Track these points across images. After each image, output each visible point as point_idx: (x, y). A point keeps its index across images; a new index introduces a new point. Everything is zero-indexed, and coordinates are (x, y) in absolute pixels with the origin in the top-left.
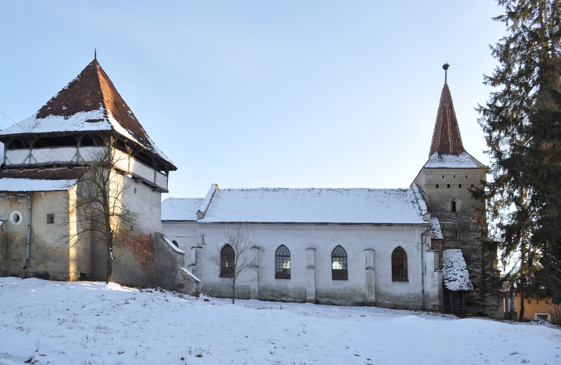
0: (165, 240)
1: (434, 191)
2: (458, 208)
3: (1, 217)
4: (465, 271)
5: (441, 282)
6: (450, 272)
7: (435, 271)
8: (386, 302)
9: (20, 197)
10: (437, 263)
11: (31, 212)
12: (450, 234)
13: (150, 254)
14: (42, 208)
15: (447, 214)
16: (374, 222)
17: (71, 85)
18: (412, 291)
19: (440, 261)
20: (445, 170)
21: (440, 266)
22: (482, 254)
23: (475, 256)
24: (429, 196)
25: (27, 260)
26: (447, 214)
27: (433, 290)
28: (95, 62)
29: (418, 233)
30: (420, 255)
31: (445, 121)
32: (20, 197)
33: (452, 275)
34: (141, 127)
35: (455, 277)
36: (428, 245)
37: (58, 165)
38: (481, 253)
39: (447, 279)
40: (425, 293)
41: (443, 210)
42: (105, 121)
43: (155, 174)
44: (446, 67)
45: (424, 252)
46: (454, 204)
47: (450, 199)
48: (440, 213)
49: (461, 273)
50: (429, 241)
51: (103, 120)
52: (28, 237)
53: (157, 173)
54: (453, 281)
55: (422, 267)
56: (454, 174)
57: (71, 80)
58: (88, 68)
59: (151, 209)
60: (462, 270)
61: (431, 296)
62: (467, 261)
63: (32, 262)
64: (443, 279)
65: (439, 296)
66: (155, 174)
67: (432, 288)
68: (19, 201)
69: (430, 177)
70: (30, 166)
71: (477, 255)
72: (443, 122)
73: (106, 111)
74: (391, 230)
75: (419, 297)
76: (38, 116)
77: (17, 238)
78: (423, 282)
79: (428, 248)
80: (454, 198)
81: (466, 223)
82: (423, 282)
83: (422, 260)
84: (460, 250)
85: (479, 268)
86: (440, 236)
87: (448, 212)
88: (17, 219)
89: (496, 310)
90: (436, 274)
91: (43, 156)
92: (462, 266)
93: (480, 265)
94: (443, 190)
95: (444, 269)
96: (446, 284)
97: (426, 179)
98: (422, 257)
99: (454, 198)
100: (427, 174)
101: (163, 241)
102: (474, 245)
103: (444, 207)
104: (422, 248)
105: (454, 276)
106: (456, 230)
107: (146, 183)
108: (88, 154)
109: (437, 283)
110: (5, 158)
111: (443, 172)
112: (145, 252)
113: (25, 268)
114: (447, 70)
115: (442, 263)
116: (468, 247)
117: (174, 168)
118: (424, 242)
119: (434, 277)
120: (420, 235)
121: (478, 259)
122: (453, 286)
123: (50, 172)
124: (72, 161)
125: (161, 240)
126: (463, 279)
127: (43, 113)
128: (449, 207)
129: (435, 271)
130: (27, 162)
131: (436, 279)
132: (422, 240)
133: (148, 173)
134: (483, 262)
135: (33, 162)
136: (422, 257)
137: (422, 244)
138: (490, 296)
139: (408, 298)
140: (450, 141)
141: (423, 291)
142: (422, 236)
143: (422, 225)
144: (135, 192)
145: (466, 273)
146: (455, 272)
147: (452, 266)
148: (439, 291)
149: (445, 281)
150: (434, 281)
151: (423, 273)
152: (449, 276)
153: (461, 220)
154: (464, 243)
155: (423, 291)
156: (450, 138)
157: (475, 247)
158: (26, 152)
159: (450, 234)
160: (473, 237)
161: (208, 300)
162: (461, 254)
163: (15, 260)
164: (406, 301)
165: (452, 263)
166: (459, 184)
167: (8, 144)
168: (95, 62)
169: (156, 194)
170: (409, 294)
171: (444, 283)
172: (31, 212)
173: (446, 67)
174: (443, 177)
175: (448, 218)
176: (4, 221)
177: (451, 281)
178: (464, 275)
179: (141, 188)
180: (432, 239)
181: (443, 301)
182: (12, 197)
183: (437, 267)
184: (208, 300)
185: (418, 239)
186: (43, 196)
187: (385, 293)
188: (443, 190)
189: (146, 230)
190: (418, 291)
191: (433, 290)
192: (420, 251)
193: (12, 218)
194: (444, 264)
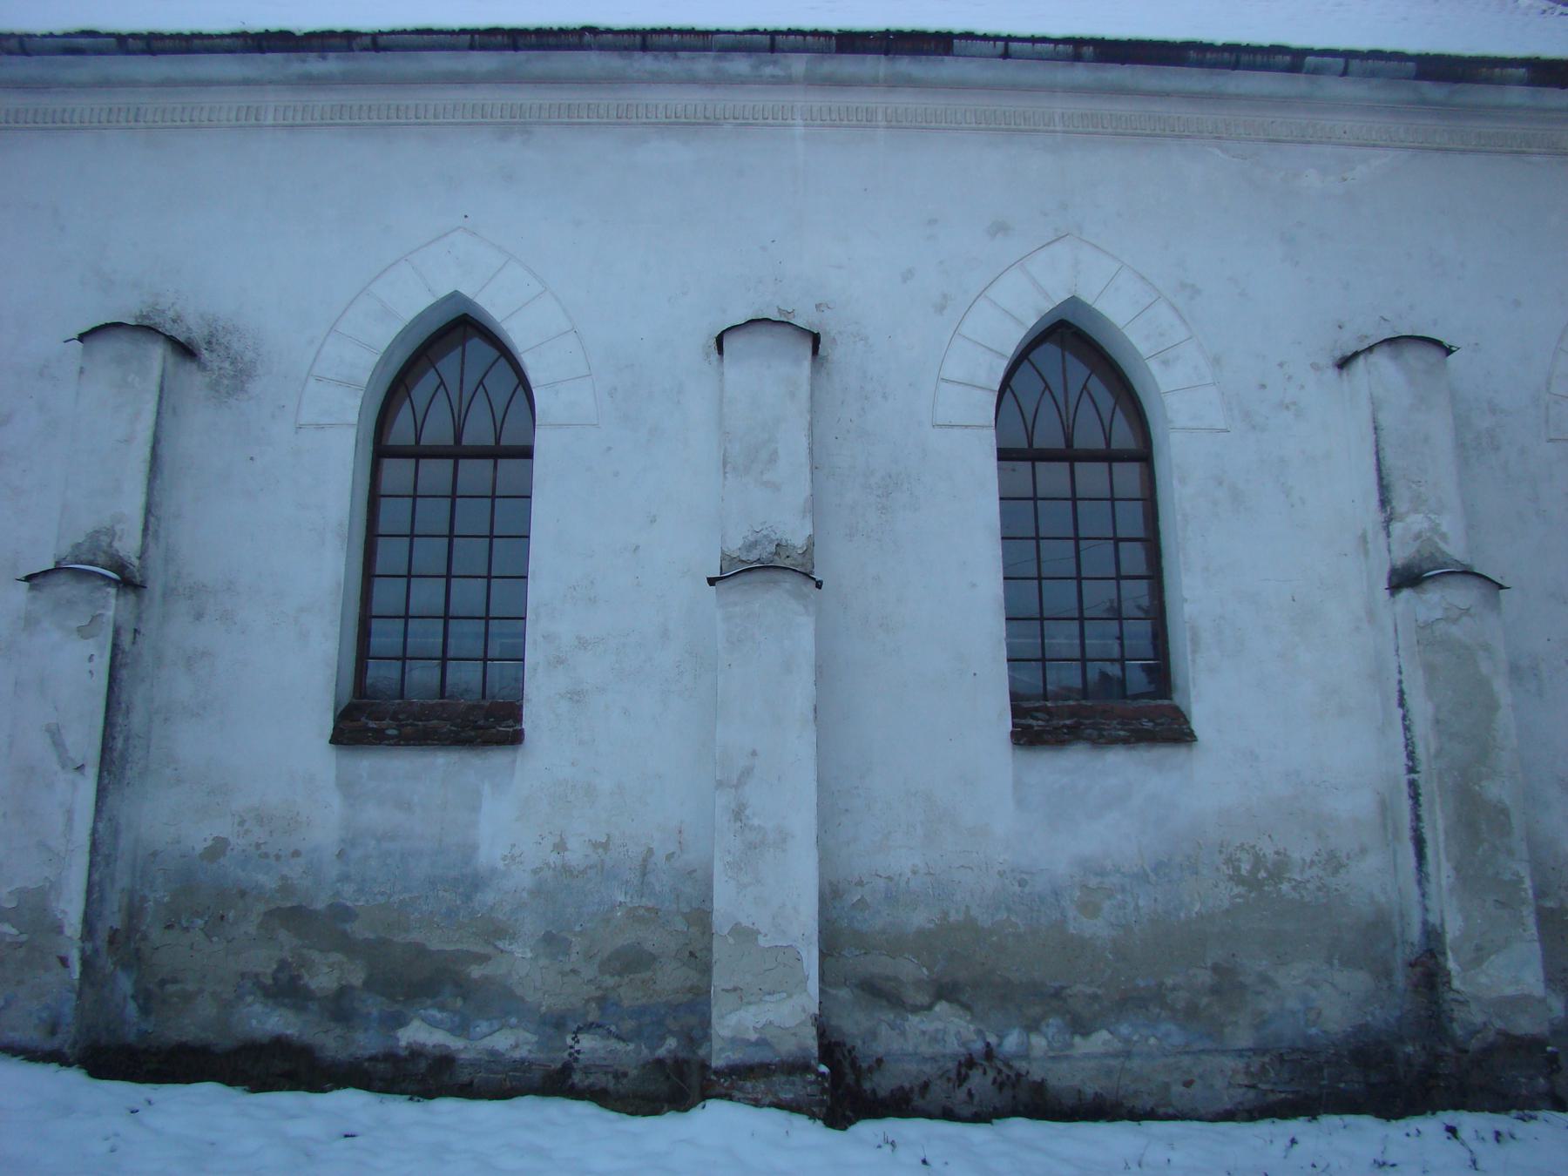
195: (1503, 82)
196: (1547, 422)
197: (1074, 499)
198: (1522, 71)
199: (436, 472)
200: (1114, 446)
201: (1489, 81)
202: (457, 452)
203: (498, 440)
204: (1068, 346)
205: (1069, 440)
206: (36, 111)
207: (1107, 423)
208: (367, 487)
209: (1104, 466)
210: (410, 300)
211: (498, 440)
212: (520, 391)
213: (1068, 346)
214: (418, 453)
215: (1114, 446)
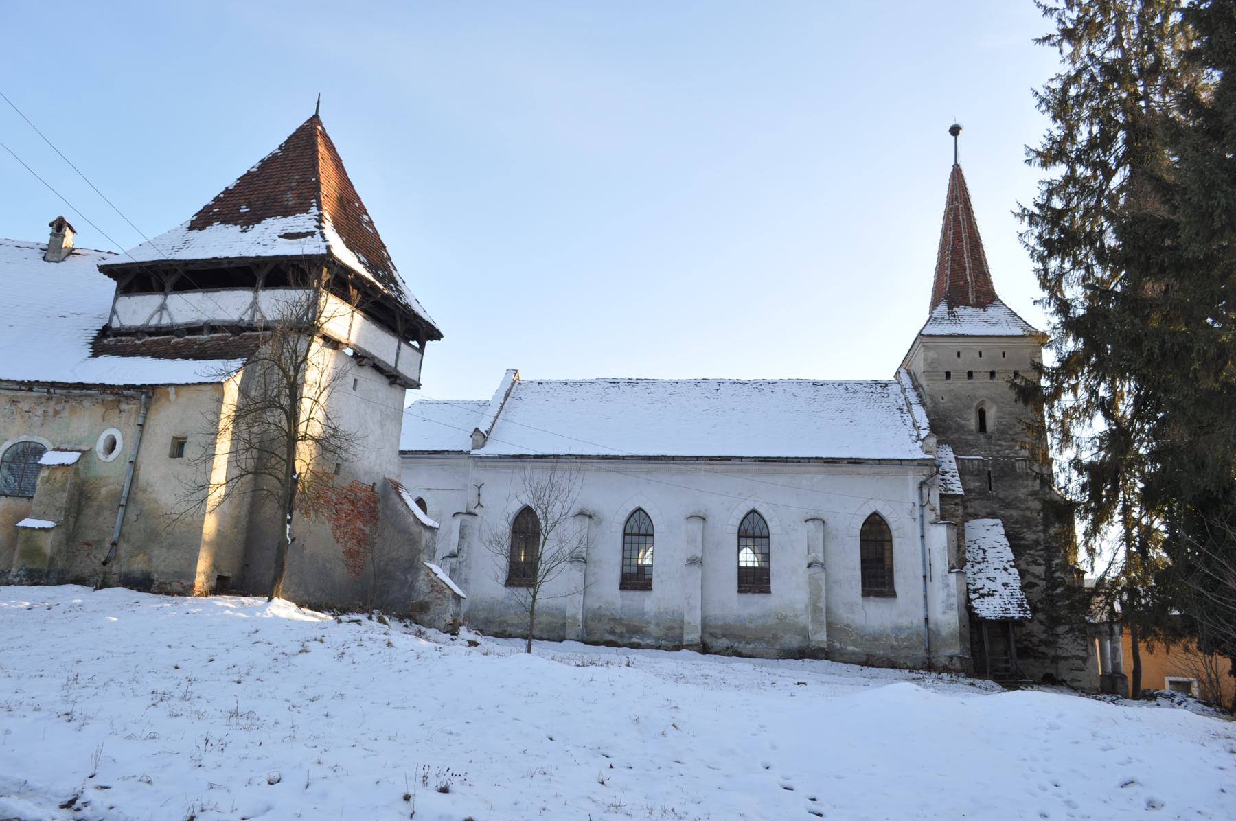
0: (401, 497)
1: (941, 385)
3: (80, 443)
4: (1012, 570)
5: (963, 598)
6: (980, 575)
7: (950, 572)
8: (850, 648)
9: (127, 397)
10: (954, 551)
11: (142, 432)
12: (977, 484)
13: (367, 530)
14: (166, 421)
15: (969, 437)
17: (265, 164)
18: (904, 622)
19: (959, 547)
20: (961, 340)
21: (959, 561)
23: (1030, 536)
25: (114, 544)
26: (969, 437)
27: (946, 617)
28: (315, 119)
29: (912, 480)
31: (958, 238)
32: (127, 397)
34: (384, 247)
35: (992, 586)
36: (933, 510)
37: (213, 328)
39: (975, 591)
40: (931, 626)
42: (318, 236)
43: (399, 347)
44: (955, 130)
45: (927, 526)
46: (982, 414)
47: (975, 404)
48: (956, 436)
49: (1002, 577)
50: (936, 501)
51: (312, 234)
52: (126, 489)
53: (403, 344)
54: (989, 595)
55: (924, 560)
56: (979, 348)
57: (265, 154)
58: (301, 130)
59: (382, 426)
60: (1006, 569)
61: (944, 632)
63: (124, 548)
66: (399, 347)
67: (944, 613)
68: (124, 406)
70: (159, 331)
71: (1034, 532)
73: (321, 215)
74: (858, 474)
75: (918, 634)
76: (191, 228)
77: (104, 491)
78: (925, 597)
79: (932, 517)
80: (982, 402)
82: (925, 597)
83: (923, 545)
84: (998, 521)
85: (1039, 565)
86: (957, 488)
87: (970, 432)
88: (112, 446)
89: (1082, 670)
91: (188, 308)
92: (1005, 559)
93: (1041, 556)
94: (959, 384)
95: (968, 565)
96: (974, 604)
98: (923, 537)
99: (982, 402)
101: (397, 500)
102: (1028, 509)
104: (922, 516)
105: (989, 584)
107: (378, 367)
108: (275, 304)
109: (954, 600)
110: (114, 312)
111: (958, 345)
112: (359, 524)
113: (104, 563)
115: (964, 552)
116: (1014, 513)
117: (436, 335)
118: (925, 501)
119: (948, 585)
120: (917, 486)
121: (1037, 542)
122: (988, 609)
123: (195, 342)
124: (241, 320)
125: (394, 496)
126: (1008, 592)
127: (202, 220)
128: (973, 423)
129: (950, 572)
130: (154, 322)
131: (953, 590)
133: (384, 346)
135: (166, 321)
136: (923, 537)
137: (922, 506)
139: (897, 639)
141: (927, 620)
142: (920, 488)
144: (354, 388)
145: (1013, 578)
146: (992, 575)
149: (972, 596)
150: (949, 596)
151: (925, 577)
152: (979, 585)
153: (998, 452)
154: (1007, 504)
155: (927, 620)
157: (1028, 513)
158: (155, 300)
159: (977, 484)
160: (1024, 491)
163: (88, 544)
164: (892, 647)
165: (984, 551)
167: (125, 283)
168: (315, 119)
169: (395, 391)
170: (898, 629)
171: (969, 600)
172: (142, 432)
173: (955, 130)
174: (959, 355)
176: (83, 452)
177: (983, 595)
179: (369, 378)
180: (942, 496)
182: (111, 398)
183: (953, 562)
185: (912, 495)
186: (172, 397)
187: (848, 626)
188: (959, 384)
189: (366, 473)
190: (915, 622)
191: (946, 617)
193: (100, 446)
194: (968, 555)
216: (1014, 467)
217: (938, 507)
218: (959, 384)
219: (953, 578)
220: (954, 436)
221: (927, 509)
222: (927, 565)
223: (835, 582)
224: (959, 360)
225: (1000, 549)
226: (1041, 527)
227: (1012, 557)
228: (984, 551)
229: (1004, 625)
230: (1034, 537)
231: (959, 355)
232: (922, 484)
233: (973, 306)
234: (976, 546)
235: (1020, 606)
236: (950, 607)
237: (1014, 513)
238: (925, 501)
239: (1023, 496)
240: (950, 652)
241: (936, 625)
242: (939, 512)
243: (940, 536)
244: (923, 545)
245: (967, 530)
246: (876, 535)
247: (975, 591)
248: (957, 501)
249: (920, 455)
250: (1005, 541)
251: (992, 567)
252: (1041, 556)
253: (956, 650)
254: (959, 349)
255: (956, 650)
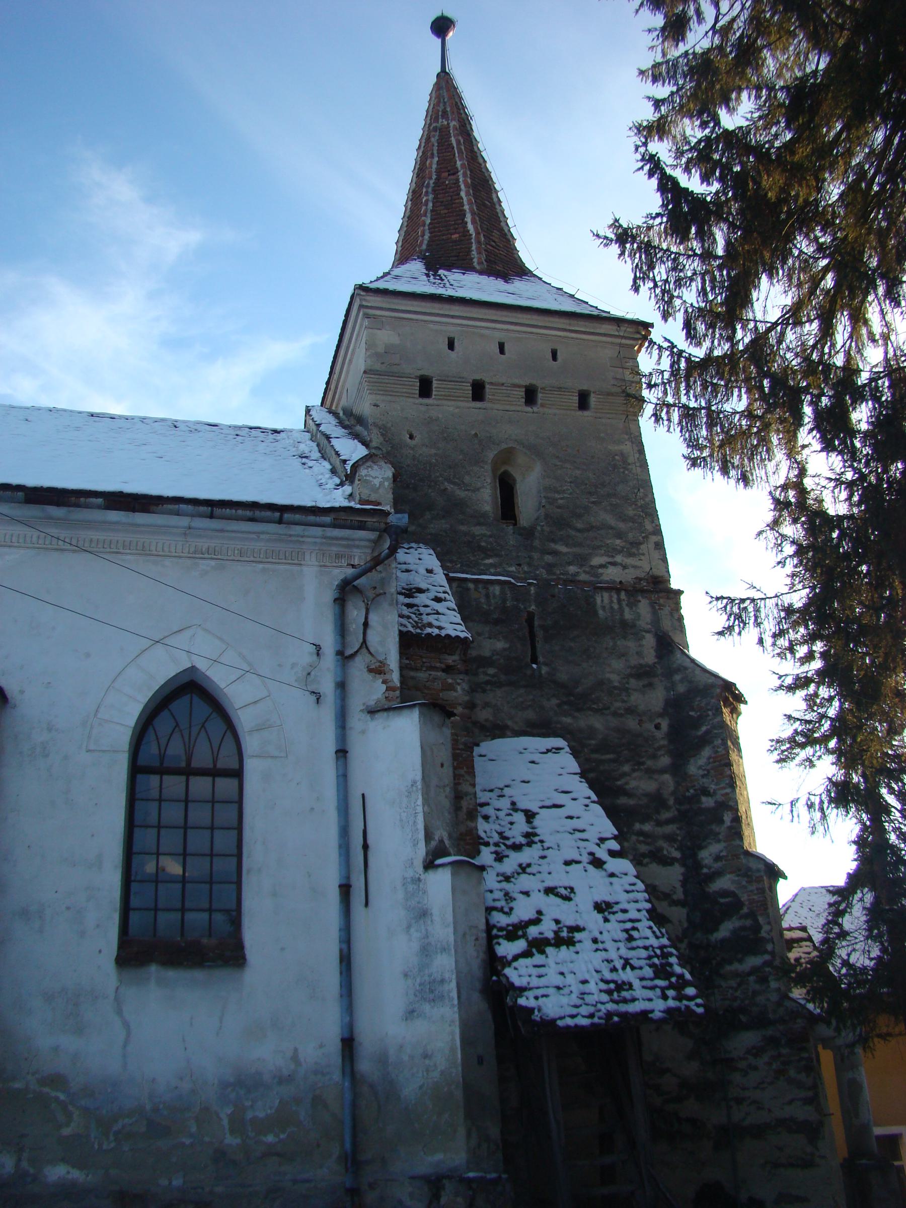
1: (410, 407)
2: (528, 505)
4: (613, 864)
5: (475, 955)
6: (525, 881)
7: (429, 865)
8: (57, 1172)
10: (445, 801)
12: (500, 645)
15: (478, 530)
16: (31, 481)
18: (268, 1055)
19: (458, 797)
20: (456, 310)
21: (460, 833)
22: (677, 769)
23: (641, 785)
24: (384, 431)
26: (478, 530)
27: (420, 1029)
29: (312, 585)
30: (330, 747)
31: (447, 167)
33: (539, 900)
35: (567, 913)
36: (378, 670)
38: (665, 761)
39: (513, 933)
40: (365, 1066)
41: (455, 508)
44: (441, 26)
45: (357, 720)
46: (506, 488)
47: (491, 455)
48: (443, 524)
49: (591, 886)
50: (386, 643)
54: (559, 941)
55: (345, 831)
56: (499, 336)
60: (598, 863)
61: (411, 1087)
62: (612, 813)
64: (491, 934)
65: (468, 1088)
67: (411, 1014)
69: (386, 337)
71: (650, 772)
72: (438, 172)
74: (144, 552)
75: (317, 1101)
78: (346, 960)
79: (376, 691)
80: (507, 456)
81: (572, 580)
82: (346, 960)
83: (343, 778)
84: (560, 742)
85: (666, 862)
86: (450, 623)
87: (480, 518)
89: (807, 1163)
90: (440, 883)
92: (592, 835)
93: (670, 838)
94: (450, 407)
95: (486, 856)
96: (517, 974)
97: (370, 346)
98: (342, 753)
99: (507, 456)
100: (376, 322)
102: (631, 711)
103: (461, 494)
104: (342, 686)
105: (554, 908)
106: (530, 618)
109: (445, 965)
111: (452, 323)
114: (438, 69)
115: (472, 815)
116: (597, 723)
118: (354, 643)
119: (423, 914)
120: (329, 595)
121: (658, 800)
122: (562, 988)
126: (614, 929)
128: (486, 498)
129: (429, 865)
131: (442, 930)
132: (342, 629)
134: (684, 817)
136: (342, 753)
137: (344, 657)
138: (756, 1052)
139: (238, 1124)
140: (470, 227)
141: (349, 1043)
142: (341, 601)
143: (338, 517)
145: (623, 882)
146: (560, 878)
147: (530, 838)
148: (466, 1042)
149: (506, 949)
150: (426, 951)
151: (345, 889)
152: (523, 910)
153: (549, 567)
154: (578, 699)
155: (349, 1043)
156: (468, 218)
157: (632, 723)
159: (500, 645)
160: (618, 664)
161: (630, 885)
162: (573, 765)
164: (221, 1155)
165: (530, 816)
166: (526, 381)
170: (245, 1083)
171: (494, 964)
173: (441, 26)
174: (451, 345)
175: (486, 552)
177: (539, 945)
178: (616, 892)
180: (407, 641)
181: (495, 1132)
183: (441, 833)
184: (630, 885)
185: (313, 619)
187: (57, 1080)
188: (451, 408)
190: (310, 1053)
191: (420, 1029)
192: (328, 714)
194: (482, 827)
195: (87, 506)
196: (89, 737)
197: (187, 801)
198: (100, 501)
199: (174, 785)
200: (219, 765)
201: (78, 505)
202: (189, 772)
203: (162, 763)
204: (188, 695)
205: (189, 761)
206: (91, 541)
207: (215, 753)
208: (244, 805)
209: (209, 779)
210: (163, 669)
211: (162, 763)
212: (229, 734)
213: (188, 695)
214: (162, 771)
215: (219, 765)
216: (591, 609)
217: (393, 661)
218: (451, 408)
219: (440, 883)
220: (439, 526)
221: (359, 665)
222: (355, 847)
223: (25, 914)
224: (453, 355)
225: (572, 808)
226: (665, 761)
227: (609, 829)
228: (530, 816)
229: (610, 1042)
230: (648, 786)
231: (451, 345)
232: (346, 591)
233: (481, 273)
234: (505, 804)
235: (662, 971)
236: (429, 991)
237: (597, 723)
238: (354, 643)
239: (615, 678)
240: (431, 1160)
241: (382, 1059)
242: (395, 678)
243: (397, 749)
244: (343, 778)
245: (478, 763)
246: (184, 742)
247: (513, 933)
248: (451, 660)
249: (338, 498)
250: (583, 790)
251: (556, 858)
252: (670, 838)
253: (452, 1154)
254: (452, 331)
255: (452, 1154)
